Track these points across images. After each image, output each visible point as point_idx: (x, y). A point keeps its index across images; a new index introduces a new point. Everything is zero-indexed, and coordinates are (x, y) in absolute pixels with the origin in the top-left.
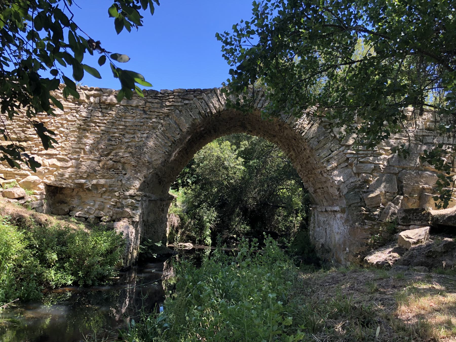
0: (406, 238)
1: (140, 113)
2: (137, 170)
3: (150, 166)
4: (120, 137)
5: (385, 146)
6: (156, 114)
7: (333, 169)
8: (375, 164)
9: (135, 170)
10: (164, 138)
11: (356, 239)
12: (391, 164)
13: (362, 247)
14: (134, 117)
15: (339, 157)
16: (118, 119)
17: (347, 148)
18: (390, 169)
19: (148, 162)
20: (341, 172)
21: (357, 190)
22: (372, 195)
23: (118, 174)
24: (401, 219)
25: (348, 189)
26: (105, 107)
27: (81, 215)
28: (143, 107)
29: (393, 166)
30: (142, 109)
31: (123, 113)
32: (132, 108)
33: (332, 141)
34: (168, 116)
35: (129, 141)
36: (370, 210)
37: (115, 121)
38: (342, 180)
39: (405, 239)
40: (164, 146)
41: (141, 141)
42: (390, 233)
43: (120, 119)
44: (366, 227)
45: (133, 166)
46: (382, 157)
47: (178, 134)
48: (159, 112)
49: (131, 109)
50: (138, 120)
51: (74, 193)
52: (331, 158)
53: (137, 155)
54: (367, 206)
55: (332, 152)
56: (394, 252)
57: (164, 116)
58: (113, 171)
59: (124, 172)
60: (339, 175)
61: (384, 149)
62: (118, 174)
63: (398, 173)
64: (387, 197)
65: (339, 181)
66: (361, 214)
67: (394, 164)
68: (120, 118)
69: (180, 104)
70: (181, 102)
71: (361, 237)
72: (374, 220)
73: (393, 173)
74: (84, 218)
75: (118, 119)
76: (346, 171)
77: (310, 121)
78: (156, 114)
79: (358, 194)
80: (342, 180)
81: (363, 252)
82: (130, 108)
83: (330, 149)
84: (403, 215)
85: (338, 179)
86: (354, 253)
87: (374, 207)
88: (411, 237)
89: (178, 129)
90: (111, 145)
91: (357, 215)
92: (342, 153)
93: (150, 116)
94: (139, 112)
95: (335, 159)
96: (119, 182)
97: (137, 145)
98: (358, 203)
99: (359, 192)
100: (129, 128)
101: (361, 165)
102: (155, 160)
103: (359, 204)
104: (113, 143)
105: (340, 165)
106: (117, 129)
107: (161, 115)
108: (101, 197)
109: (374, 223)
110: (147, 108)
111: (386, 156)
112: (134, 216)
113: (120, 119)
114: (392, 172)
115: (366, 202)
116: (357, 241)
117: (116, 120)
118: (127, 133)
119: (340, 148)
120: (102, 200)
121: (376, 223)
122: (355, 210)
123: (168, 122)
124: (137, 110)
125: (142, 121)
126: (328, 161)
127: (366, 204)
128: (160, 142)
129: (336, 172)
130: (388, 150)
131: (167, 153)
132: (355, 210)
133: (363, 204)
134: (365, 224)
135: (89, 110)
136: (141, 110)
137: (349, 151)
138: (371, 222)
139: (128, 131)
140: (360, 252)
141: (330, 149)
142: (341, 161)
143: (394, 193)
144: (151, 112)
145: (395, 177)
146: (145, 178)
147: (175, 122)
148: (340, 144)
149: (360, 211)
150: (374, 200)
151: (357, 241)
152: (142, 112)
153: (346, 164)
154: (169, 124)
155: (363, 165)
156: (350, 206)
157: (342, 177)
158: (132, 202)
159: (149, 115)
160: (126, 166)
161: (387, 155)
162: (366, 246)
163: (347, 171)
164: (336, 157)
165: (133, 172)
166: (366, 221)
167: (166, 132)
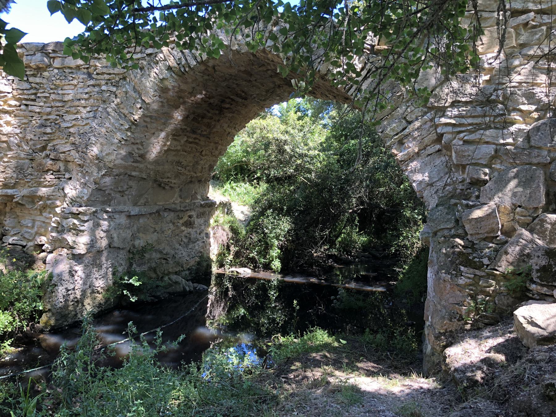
0: (529, 323)
1: (83, 79)
2: (84, 172)
3: (101, 165)
4: (56, 120)
5: (524, 104)
6: (107, 77)
7: (411, 158)
8: (497, 145)
9: (82, 172)
10: (118, 117)
11: (443, 302)
12: (533, 143)
13: (451, 321)
14: (76, 85)
15: (424, 132)
16: (52, 91)
17: (440, 114)
18: (530, 153)
19: (98, 159)
20: (426, 165)
21: (453, 201)
22: (478, 213)
23: (59, 178)
24: (538, 271)
25: (440, 198)
26: (32, 73)
27: (14, 242)
28: (87, 68)
29: (539, 148)
30: (85, 71)
31: (58, 81)
32: (70, 71)
33: (408, 101)
34: (124, 78)
35: (70, 125)
36: (474, 244)
37: (48, 95)
38: (427, 179)
39: (525, 325)
40: (120, 130)
41: (86, 124)
42: (515, 298)
43: (56, 91)
44: (462, 281)
45: (80, 165)
46: (513, 129)
47: (140, 108)
48: (110, 74)
49: (70, 73)
50: (80, 90)
51: (8, 209)
52: (407, 136)
53: (82, 149)
54: (469, 237)
55: (409, 123)
56: (499, 352)
57: (117, 79)
58: (52, 174)
59: (67, 176)
60: (421, 171)
61: (521, 111)
62: (59, 178)
63: (550, 163)
64: (517, 217)
65: (421, 182)
66: (454, 253)
67: (540, 144)
68: (55, 89)
69: (139, 56)
70: (141, 52)
71: (451, 300)
72: (480, 266)
73: (538, 164)
74: (20, 245)
75: (52, 91)
76: (438, 162)
77: (366, 64)
78: (107, 77)
79: (453, 210)
80: (427, 179)
81: (451, 331)
82: (67, 71)
83: (405, 118)
84: (544, 263)
85: (419, 177)
86: (437, 332)
87: (485, 239)
88: (539, 323)
89: (139, 100)
90: (45, 133)
91: (445, 254)
92: (429, 124)
93: (98, 82)
94: (82, 76)
95: (414, 139)
96: (61, 191)
97: (81, 132)
98: (450, 229)
99: (456, 204)
100: (69, 104)
101: (466, 147)
102: (107, 155)
103: (453, 231)
104: (48, 130)
105: (425, 148)
106: (52, 107)
107: (114, 78)
108: (41, 214)
109: (478, 272)
110: (92, 68)
111: (523, 126)
112: (75, 246)
113: (56, 91)
114: (535, 161)
115: (467, 227)
116: (445, 307)
117: (50, 94)
118: (67, 112)
119: (425, 113)
120: (42, 219)
121: (483, 274)
122: (444, 242)
123: (124, 90)
124: (79, 73)
125: (86, 91)
126: (401, 143)
127: (466, 234)
128: (113, 125)
129: (414, 164)
130: (531, 112)
131: (123, 143)
132: (444, 242)
133: (460, 231)
134: (460, 274)
135: (9, 80)
136: (84, 73)
137: (443, 120)
138: (472, 270)
139: (68, 109)
140: (446, 332)
141: (405, 118)
142: (426, 141)
143: (536, 209)
144: (98, 74)
145: (540, 174)
146: (96, 183)
147: (134, 87)
148: (425, 106)
149: (453, 247)
150: (483, 223)
151: (445, 307)
152: (85, 76)
153: (438, 147)
154: (126, 93)
155: (472, 148)
156: (435, 234)
157: (427, 174)
158: (74, 224)
159: (96, 79)
160: (71, 166)
161: (527, 124)
162: (459, 320)
163: (439, 161)
164: (416, 134)
165: (80, 174)
166: (462, 268)
167: (122, 106)
